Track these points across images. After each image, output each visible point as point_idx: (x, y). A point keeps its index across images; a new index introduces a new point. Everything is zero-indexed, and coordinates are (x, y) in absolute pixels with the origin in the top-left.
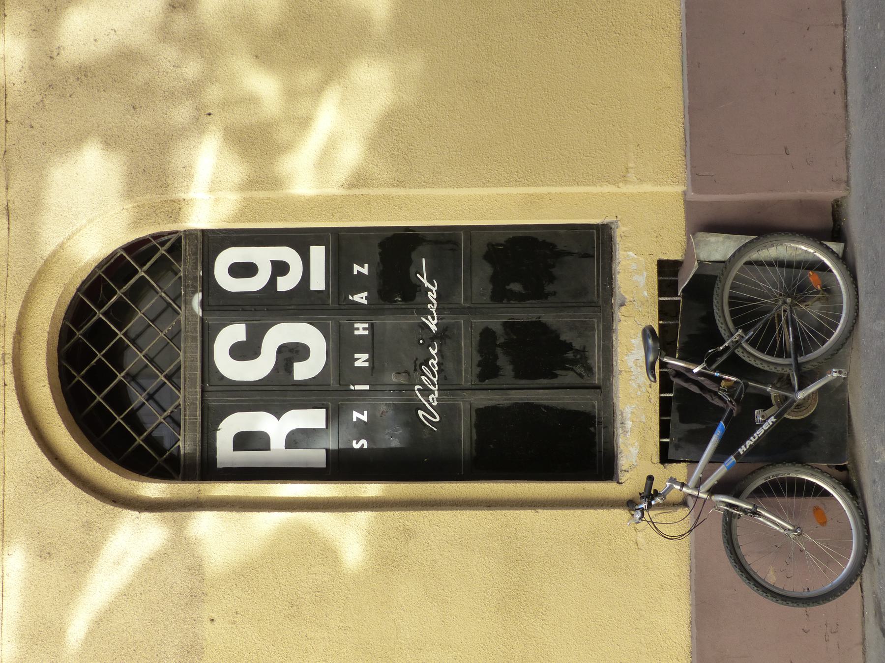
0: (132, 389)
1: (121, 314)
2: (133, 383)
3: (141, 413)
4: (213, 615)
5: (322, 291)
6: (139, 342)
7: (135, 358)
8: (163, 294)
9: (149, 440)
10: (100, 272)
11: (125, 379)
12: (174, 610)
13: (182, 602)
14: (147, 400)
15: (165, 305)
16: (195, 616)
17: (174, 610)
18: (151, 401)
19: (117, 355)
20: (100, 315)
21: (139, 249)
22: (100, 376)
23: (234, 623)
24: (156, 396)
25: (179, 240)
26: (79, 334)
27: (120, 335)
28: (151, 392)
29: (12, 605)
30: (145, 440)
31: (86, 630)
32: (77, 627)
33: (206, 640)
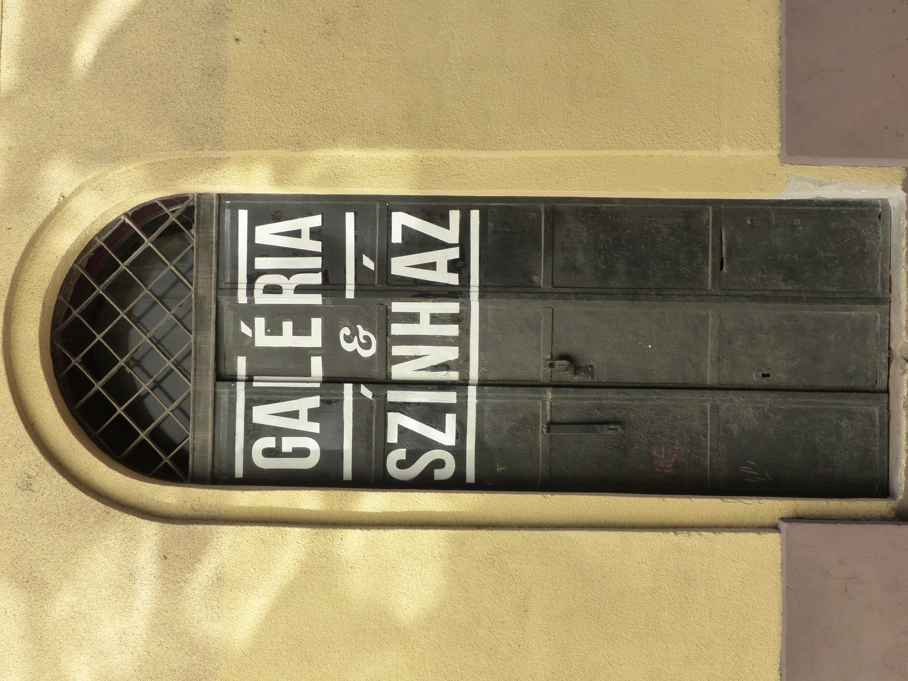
0: (136, 375)
1: (123, 289)
2: (137, 369)
3: (148, 401)
4: (238, 34)
5: (356, 215)
6: (144, 321)
7: (140, 340)
8: (172, 268)
9: (158, 435)
10: (100, 242)
11: (128, 365)
12: (194, 29)
13: (204, 20)
14: (152, 390)
15: (175, 279)
16: (217, 35)
17: (194, 29)
18: (157, 390)
19: (119, 338)
20: (99, 290)
21: (147, 215)
22: (98, 362)
23: (262, 42)
24: (164, 384)
25: (190, 210)
26: (75, 313)
27: (122, 314)
28: (158, 379)
29: (13, 25)
30: (152, 435)
31: (94, 52)
32: (86, 49)
33: (230, 62)
